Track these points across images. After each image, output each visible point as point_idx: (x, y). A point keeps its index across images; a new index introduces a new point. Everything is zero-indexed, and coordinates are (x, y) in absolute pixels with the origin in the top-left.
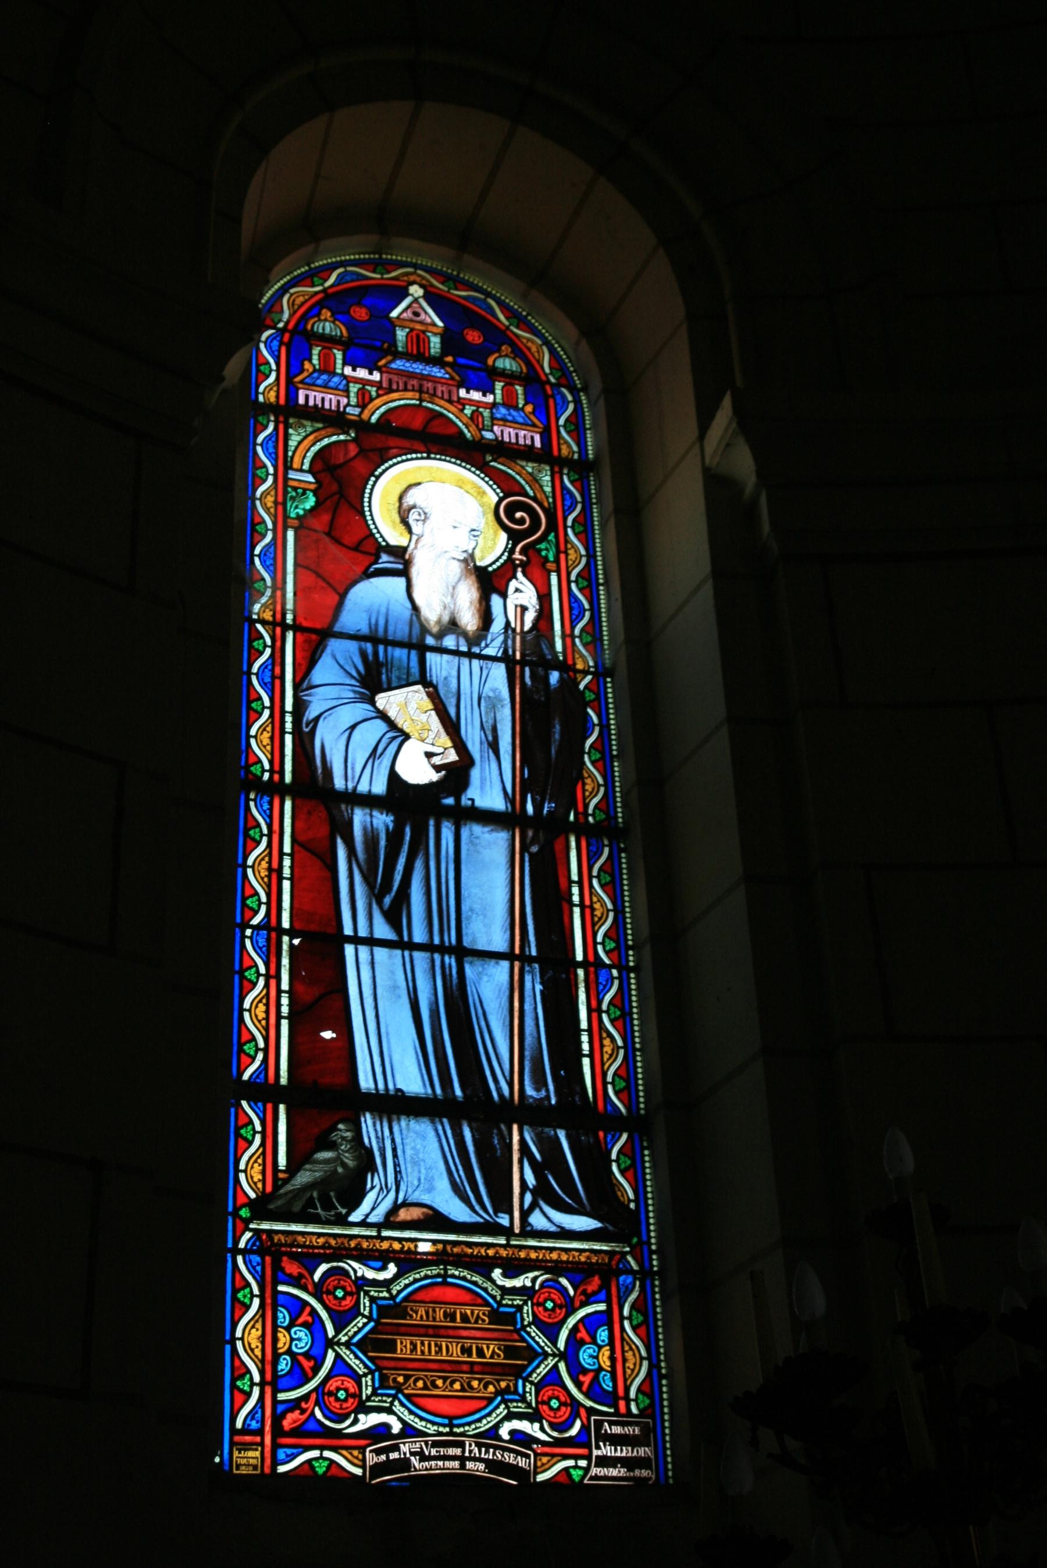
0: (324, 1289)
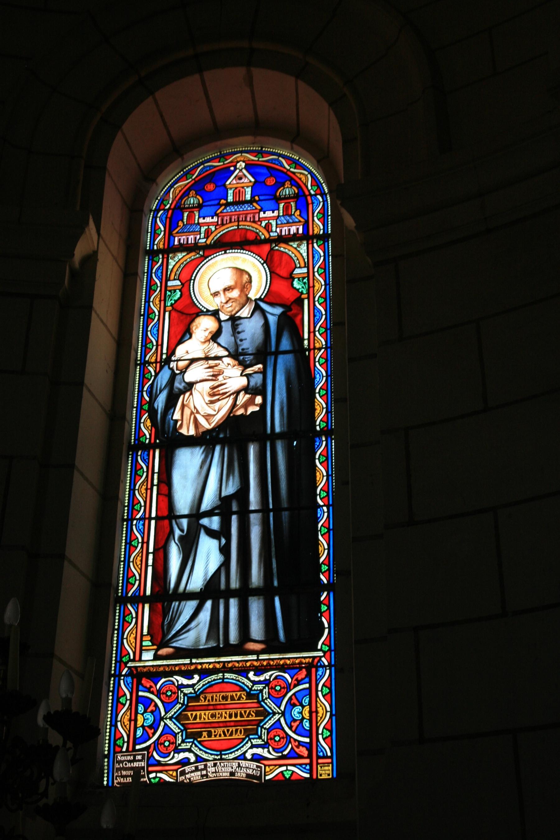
0: (161, 692)
